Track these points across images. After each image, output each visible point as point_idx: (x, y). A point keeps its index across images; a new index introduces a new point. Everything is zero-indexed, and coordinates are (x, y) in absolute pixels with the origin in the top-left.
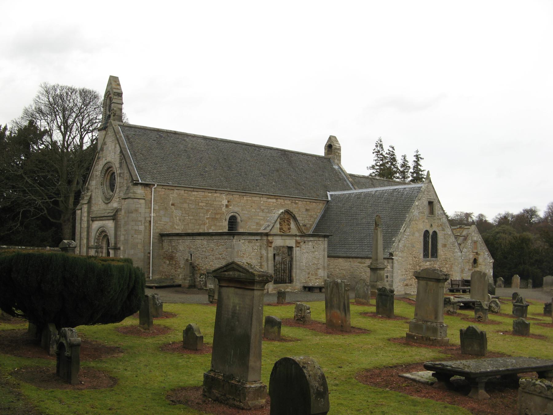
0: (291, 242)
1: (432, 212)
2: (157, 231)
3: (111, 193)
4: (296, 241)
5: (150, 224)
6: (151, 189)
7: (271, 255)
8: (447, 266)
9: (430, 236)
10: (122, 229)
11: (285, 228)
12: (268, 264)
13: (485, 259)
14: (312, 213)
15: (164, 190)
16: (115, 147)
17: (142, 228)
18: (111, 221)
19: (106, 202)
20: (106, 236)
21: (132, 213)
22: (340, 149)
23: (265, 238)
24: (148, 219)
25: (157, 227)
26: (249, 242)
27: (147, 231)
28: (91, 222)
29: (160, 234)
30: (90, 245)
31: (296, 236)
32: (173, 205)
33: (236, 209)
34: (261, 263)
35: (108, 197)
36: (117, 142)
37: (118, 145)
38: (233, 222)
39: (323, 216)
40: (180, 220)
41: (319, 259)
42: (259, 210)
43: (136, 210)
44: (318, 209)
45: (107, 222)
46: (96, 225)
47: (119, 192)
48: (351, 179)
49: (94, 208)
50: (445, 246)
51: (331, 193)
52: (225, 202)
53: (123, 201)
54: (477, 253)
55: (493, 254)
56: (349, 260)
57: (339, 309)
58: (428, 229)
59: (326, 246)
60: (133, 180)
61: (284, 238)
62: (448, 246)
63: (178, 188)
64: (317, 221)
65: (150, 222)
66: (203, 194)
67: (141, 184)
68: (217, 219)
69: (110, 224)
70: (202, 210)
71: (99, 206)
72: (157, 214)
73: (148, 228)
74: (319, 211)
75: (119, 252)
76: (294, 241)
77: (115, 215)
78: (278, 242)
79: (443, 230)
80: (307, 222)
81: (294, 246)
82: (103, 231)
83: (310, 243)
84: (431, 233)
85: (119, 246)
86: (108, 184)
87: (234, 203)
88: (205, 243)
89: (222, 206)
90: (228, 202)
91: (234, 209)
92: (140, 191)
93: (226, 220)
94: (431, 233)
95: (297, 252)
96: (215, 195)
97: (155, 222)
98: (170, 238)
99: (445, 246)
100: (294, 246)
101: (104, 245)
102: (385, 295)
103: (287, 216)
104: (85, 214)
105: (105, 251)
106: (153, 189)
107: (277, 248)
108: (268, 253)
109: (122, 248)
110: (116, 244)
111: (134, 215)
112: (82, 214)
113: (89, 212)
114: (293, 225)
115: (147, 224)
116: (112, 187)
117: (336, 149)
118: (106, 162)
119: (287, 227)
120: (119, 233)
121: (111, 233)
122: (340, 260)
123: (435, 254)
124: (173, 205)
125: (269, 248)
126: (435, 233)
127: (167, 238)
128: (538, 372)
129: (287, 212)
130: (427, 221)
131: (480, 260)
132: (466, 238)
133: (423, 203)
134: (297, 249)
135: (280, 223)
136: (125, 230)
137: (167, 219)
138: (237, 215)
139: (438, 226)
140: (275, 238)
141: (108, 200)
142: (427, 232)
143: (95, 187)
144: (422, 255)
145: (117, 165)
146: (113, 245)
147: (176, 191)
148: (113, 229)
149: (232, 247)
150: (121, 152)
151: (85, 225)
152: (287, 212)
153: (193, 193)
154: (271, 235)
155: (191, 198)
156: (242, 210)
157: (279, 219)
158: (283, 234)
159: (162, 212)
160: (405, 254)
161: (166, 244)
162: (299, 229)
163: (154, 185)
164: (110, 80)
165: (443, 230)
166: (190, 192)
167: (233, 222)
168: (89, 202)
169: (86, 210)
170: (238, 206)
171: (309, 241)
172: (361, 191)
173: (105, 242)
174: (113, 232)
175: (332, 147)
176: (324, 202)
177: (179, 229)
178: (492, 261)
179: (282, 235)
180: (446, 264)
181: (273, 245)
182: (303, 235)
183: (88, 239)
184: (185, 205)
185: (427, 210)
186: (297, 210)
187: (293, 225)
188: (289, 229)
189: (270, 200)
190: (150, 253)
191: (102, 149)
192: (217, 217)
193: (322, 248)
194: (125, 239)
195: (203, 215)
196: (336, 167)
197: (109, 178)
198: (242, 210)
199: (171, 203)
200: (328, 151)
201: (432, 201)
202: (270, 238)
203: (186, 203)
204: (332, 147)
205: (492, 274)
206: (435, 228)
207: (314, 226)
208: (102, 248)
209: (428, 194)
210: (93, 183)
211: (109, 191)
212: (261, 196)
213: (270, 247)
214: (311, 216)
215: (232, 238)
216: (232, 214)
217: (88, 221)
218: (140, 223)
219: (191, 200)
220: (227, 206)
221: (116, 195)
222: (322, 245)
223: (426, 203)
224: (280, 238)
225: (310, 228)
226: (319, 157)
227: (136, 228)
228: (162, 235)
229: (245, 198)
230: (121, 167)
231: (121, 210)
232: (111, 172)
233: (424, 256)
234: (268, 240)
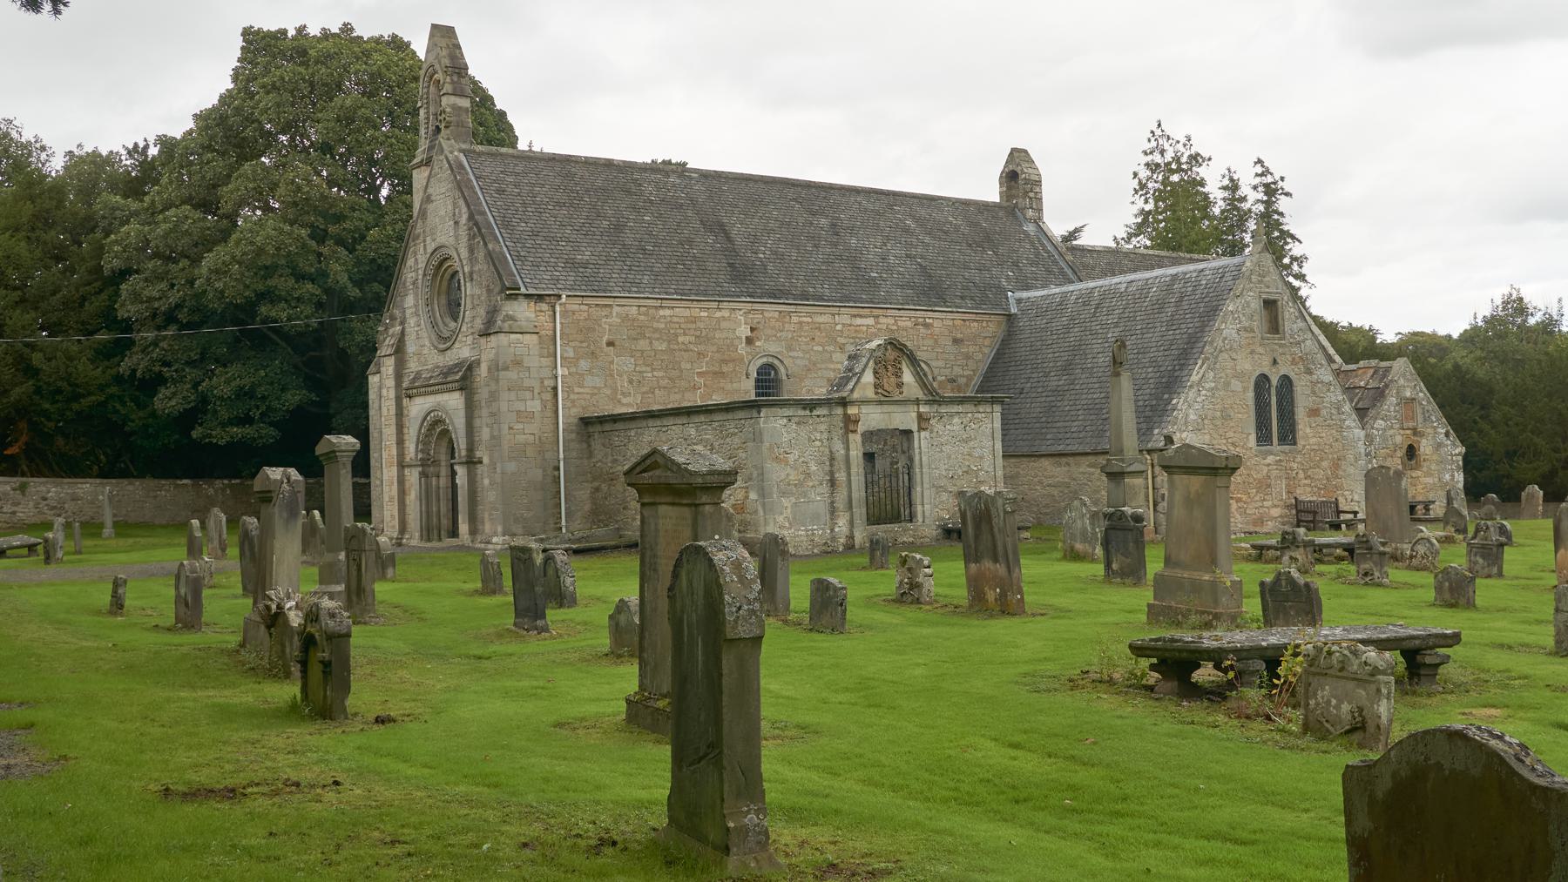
0: (905, 418)
1: (1274, 326)
2: (574, 411)
3: (453, 325)
4: (920, 417)
5: (556, 395)
6: (553, 307)
7: (856, 453)
8: (1325, 464)
9: (1273, 391)
10: (484, 412)
11: (889, 382)
12: (849, 475)
13: (1439, 445)
14: (971, 349)
15: (585, 308)
16: (455, 205)
17: (535, 406)
18: (457, 395)
19: (442, 346)
20: (445, 432)
21: (506, 369)
22: (1038, 183)
23: (839, 411)
24: (551, 383)
25: (573, 401)
26: (798, 423)
27: (549, 413)
28: (405, 401)
29: (582, 419)
30: (408, 459)
31: (917, 402)
32: (610, 344)
33: (773, 348)
34: (832, 473)
35: (446, 334)
36: (458, 194)
37: (461, 202)
38: (768, 381)
39: (999, 355)
40: (631, 382)
41: (981, 458)
42: (831, 348)
43: (518, 363)
44: (984, 332)
45: (446, 396)
46: (418, 407)
47: (472, 316)
48: (1069, 257)
49: (413, 366)
50: (1314, 412)
51: (1019, 294)
52: (744, 331)
53: (483, 340)
54: (1415, 432)
55: (1461, 429)
56: (1064, 460)
57: (996, 560)
58: (1266, 371)
59: (998, 424)
60: (504, 288)
61: (886, 408)
62: (1324, 412)
63: (623, 301)
64: (983, 367)
65: (555, 389)
66: (687, 313)
67: (527, 296)
68: (721, 374)
69: (453, 402)
70: (686, 355)
71: (423, 354)
72: (573, 370)
73: (549, 405)
74: (987, 342)
75: (480, 469)
76: (914, 415)
77: (464, 378)
78: (873, 418)
79: (1309, 372)
80: (957, 371)
81: (915, 428)
82: (438, 421)
83: (956, 420)
84: (1274, 381)
85: (478, 454)
86: (444, 301)
87: (769, 332)
88: (693, 432)
89: (736, 342)
90: (752, 329)
91: (770, 346)
92: (523, 311)
93: (747, 376)
94: (1274, 381)
95: (922, 441)
96: (718, 314)
97: (569, 390)
98: (607, 427)
99: (1314, 412)
100: (915, 428)
101: (443, 457)
102: (1124, 529)
103: (891, 354)
104: (391, 383)
105: (444, 471)
106: (558, 308)
107: (869, 436)
108: (848, 449)
109: (486, 460)
110: (471, 449)
111: (512, 375)
112: (381, 385)
113: (399, 377)
114: (908, 377)
115: (548, 396)
116: (453, 308)
117: (1027, 181)
118: (433, 246)
119: (893, 379)
120: (477, 422)
121: (458, 424)
122: (1045, 462)
123: (1288, 434)
124: (610, 344)
125: (851, 436)
126: (1286, 382)
127: (598, 428)
128: (1403, 653)
129: (893, 344)
130: (1260, 350)
131: (1425, 447)
132: (1380, 394)
133: (1248, 303)
134: (923, 434)
135: (875, 372)
136: (493, 415)
137: (598, 382)
138: (776, 362)
139: (1294, 362)
140: (865, 409)
141: (445, 341)
142: (1262, 382)
143: (411, 310)
144: (1253, 437)
145: (464, 253)
146: (464, 453)
147: (616, 309)
148: (462, 413)
149: (757, 437)
150: (471, 217)
151: (389, 407)
152: (893, 344)
153: (662, 312)
154: (852, 403)
155: (655, 325)
156: (790, 349)
157: (871, 363)
158: (884, 397)
159: (584, 364)
160: (1207, 437)
161: (597, 444)
162: (923, 385)
163: (559, 297)
164: (432, 36)
165: (1309, 372)
166: (652, 311)
167: (768, 381)
168: (399, 350)
169: (391, 370)
170: (779, 339)
171: (952, 416)
172: (1091, 284)
173: (443, 450)
174: (463, 420)
175: (1019, 177)
176: (1000, 318)
177: (629, 404)
178: (1461, 449)
179: (880, 403)
180: (1322, 459)
181: (861, 428)
182: (935, 399)
183: (400, 442)
184: (643, 344)
185: (1259, 323)
186: (931, 342)
187: (908, 377)
188: (900, 385)
189: (859, 321)
190: (558, 469)
191: (423, 214)
192: (725, 369)
193: (988, 431)
194: (493, 437)
195: (689, 366)
196: (1030, 228)
197: (445, 283)
198: (790, 349)
199: (605, 340)
200: (1009, 188)
201: (1272, 297)
202: (852, 411)
203: (644, 337)
204: (1019, 177)
205: (1461, 485)
206: (1284, 369)
207: (977, 380)
208: (436, 463)
209: (1260, 282)
210: (410, 301)
211: (448, 319)
212: (835, 310)
213: (855, 432)
214: (968, 357)
215: (755, 414)
216: (765, 360)
217: (398, 400)
218: (528, 394)
219: (656, 330)
220: (749, 341)
221: (464, 328)
222: (990, 422)
223: (1256, 305)
224: (878, 409)
225: (967, 385)
226: (995, 205)
227: (520, 406)
228: (586, 422)
229: (795, 319)
230: (472, 259)
231: (478, 362)
232: (450, 271)
233: (1258, 439)
234: (845, 414)
